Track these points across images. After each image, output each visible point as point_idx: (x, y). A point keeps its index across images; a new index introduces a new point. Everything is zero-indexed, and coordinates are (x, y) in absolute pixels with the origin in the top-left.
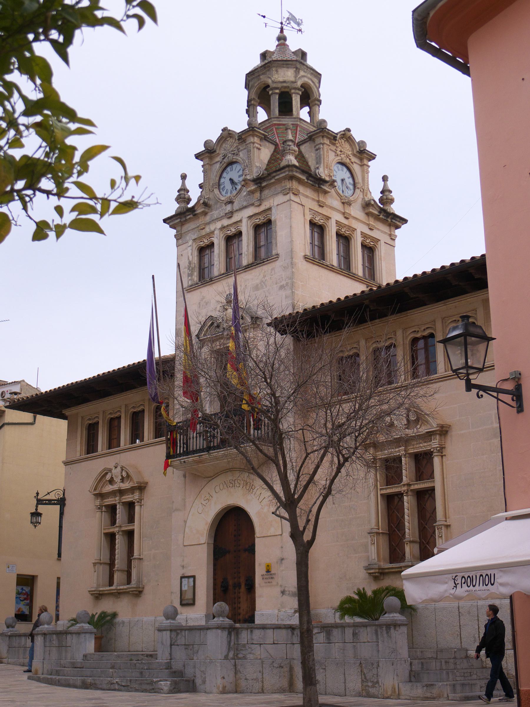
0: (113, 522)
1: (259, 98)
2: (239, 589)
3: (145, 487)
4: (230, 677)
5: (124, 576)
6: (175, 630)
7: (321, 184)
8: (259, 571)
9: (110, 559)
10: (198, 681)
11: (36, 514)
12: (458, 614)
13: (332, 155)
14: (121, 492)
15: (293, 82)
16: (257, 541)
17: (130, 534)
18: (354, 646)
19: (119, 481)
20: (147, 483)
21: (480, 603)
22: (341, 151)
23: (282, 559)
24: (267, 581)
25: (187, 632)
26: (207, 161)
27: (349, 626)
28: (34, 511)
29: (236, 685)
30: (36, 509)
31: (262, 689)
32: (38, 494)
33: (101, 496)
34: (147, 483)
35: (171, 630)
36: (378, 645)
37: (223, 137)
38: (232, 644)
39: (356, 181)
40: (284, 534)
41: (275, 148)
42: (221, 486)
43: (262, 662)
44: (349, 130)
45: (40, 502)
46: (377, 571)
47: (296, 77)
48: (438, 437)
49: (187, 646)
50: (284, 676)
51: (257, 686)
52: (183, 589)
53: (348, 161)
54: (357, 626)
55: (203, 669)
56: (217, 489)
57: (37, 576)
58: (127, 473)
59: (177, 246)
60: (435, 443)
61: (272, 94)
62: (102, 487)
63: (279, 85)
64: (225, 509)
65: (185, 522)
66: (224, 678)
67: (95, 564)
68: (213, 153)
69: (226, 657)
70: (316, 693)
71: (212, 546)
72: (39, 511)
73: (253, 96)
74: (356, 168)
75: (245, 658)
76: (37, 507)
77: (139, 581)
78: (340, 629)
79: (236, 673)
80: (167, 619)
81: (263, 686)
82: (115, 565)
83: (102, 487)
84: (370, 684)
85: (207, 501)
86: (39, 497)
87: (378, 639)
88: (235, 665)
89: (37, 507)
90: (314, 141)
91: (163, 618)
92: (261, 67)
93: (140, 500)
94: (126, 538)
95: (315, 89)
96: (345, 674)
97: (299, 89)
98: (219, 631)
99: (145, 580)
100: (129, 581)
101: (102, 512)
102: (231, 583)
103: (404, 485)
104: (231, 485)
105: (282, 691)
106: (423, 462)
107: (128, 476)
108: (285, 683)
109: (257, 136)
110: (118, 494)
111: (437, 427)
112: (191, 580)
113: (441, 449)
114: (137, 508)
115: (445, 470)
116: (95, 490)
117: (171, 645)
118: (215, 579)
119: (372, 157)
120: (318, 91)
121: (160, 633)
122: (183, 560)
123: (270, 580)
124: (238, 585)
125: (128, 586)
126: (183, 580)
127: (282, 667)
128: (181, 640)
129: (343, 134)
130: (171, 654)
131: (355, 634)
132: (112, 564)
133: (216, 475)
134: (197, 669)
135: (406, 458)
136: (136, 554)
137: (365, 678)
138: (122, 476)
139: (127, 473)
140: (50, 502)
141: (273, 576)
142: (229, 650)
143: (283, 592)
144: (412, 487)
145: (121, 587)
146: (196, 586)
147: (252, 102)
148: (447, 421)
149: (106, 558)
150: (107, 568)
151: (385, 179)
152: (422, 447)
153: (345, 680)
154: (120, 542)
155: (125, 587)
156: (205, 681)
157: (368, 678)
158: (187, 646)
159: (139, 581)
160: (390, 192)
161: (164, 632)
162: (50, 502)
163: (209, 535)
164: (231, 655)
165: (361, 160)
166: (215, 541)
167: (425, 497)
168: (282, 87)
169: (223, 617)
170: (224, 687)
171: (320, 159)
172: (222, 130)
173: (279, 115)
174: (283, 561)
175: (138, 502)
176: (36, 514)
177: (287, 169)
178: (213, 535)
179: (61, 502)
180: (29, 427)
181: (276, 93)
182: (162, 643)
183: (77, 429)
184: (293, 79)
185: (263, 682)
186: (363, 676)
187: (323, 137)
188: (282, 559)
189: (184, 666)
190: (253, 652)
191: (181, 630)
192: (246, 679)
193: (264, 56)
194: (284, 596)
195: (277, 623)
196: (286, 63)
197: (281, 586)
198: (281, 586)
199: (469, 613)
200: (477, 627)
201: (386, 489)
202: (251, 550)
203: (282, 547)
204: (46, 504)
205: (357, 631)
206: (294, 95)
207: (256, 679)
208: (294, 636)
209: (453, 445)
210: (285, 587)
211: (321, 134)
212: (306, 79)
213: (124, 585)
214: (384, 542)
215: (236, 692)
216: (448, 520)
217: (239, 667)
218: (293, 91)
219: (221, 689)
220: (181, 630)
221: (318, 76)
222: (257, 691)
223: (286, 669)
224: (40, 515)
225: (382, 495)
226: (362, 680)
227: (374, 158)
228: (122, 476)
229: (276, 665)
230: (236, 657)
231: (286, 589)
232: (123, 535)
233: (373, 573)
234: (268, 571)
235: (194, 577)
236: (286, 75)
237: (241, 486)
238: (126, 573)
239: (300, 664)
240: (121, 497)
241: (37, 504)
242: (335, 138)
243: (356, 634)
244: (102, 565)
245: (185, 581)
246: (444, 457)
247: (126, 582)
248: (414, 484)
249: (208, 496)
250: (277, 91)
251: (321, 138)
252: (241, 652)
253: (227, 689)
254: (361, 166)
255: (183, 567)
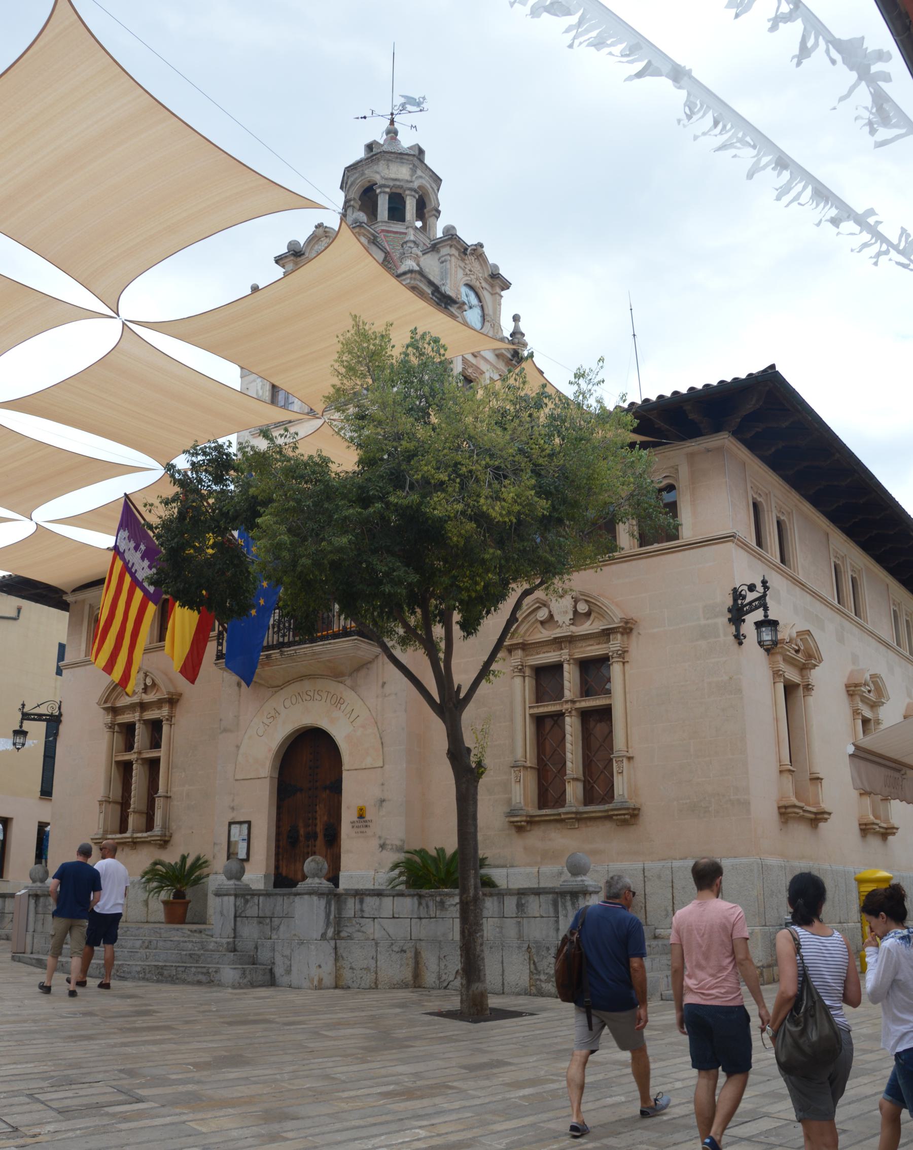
0: (129, 747)
1: (360, 199)
2: (315, 841)
3: (178, 700)
4: (329, 966)
5: (143, 820)
6: (243, 896)
7: (449, 304)
8: (348, 816)
9: (123, 797)
10: (279, 971)
11: (20, 733)
12: (642, 878)
13: (460, 273)
14: (143, 706)
15: (407, 181)
16: (345, 775)
17: (153, 764)
18: (519, 922)
19: (141, 691)
20: (180, 695)
21: (676, 864)
22: (470, 271)
23: (382, 801)
24: (359, 830)
25: (261, 898)
26: (290, 266)
27: (511, 894)
28: (18, 728)
29: (336, 977)
30: (21, 727)
31: (376, 983)
32: (23, 705)
33: (114, 711)
34: (180, 695)
35: (236, 896)
36: (557, 922)
37: (316, 236)
38: (332, 917)
39: (486, 312)
40: (386, 766)
41: (386, 257)
42: (294, 698)
43: (377, 944)
44: (481, 246)
45: (26, 716)
46: (524, 818)
47: (412, 176)
48: (619, 636)
49: (261, 919)
50: (408, 964)
51: (369, 978)
52: (232, 839)
53: (478, 284)
54: (523, 894)
55: (287, 952)
56: (288, 703)
57: (11, 819)
58: (153, 681)
59: (241, 377)
60: (615, 644)
61: (380, 192)
62: (115, 699)
63: (391, 183)
64: (298, 730)
65: (238, 747)
66: (320, 966)
67: (101, 803)
68: (300, 256)
69: (323, 936)
70: (483, 996)
71: (276, 780)
72: (25, 728)
73: (352, 195)
74: (486, 295)
75: (350, 937)
76: (22, 723)
77: (165, 826)
78: (495, 898)
79: (336, 960)
80: (229, 878)
81: (376, 979)
82: (130, 805)
83: (115, 699)
84: (543, 977)
85: (271, 720)
86: (25, 710)
87: (558, 913)
88: (336, 948)
89: (22, 723)
90: (438, 251)
91: (224, 877)
92: (367, 159)
93: (170, 718)
94: (147, 767)
95: (432, 196)
96: (502, 963)
97: (415, 191)
98: (315, 898)
99: (174, 826)
100: (149, 826)
101: (524, 677)
102: (302, 832)
103: (567, 702)
104: (308, 698)
105: (404, 985)
106: (594, 671)
107: (154, 684)
108: (408, 974)
109: (364, 235)
110: (138, 709)
111: (621, 622)
112: (245, 826)
113: (623, 654)
114: (165, 728)
115: (627, 682)
116: (106, 702)
117: (235, 917)
118: (278, 827)
119: (506, 285)
120: (437, 196)
121: (218, 900)
122: (233, 800)
123: (364, 829)
124: (313, 836)
125: (149, 833)
126: (233, 826)
127: (405, 952)
128: (252, 911)
129: (474, 250)
130: (235, 930)
131: (520, 906)
132: (124, 804)
133: (288, 683)
134: (277, 953)
135: (569, 664)
136: (161, 791)
137: (536, 969)
138: (145, 684)
139: (153, 681)
140: (39, 717)
141: (368, 824)
142: (328, 924)
143: (383, 846)
144: (578, 705)
145: (139, 835)
146: (252, 835)
147: (352, 203)
148: (632, 614)
149: (117, 794)
150: (118, 808)
151: (516, 318)
152: (593, 650)
153: (503, 971)
154: (138, 774)
155: (145, 835)
156: (291, 970)
157: (539, 969)
158: (261, 919)
159: (165, 826)
160: (523, 335)
161: (226, 898)
162: (39, 717)
163: (273, 766)
164: (330, 932)
165: (492, 286)
166: (280, 774)
167: (598, 719)
168: (394, 186)
169: (319, 877)
170: (320, 980)
171: (446, 274)
172: (316, 227)
173: (389, 219)
174: (384, 804)
175: (167, 720)
176: (20, 733)
177: (409, 275)
178: (278, 766)
179: (53, 722)
180: (11, 622)
181: (385, 192)
182: (222, 914)
183: (82, 621)
184: (408, 177)
185: (376, 973)
186: (532, 966)
187: (451, 246)
188: (382, 801)
189: (256, 948)
190: (363, 929)
191: (253, 895)
192: (351, 968)
193: (370, 147)
194: (384, 851)
195: (372, 887)
196: (401, 156)
197: (380, 837)
198: (380, 837)
199: (659, 877)
200: (671, 897)
201: (538, 707)
202: (336, 787)
203: (383, 784)
204: (34, 720)
205: (523, 902)
206: (408, 198)
207: (367, 969)
208: (421, 908)
209: (638, 648)
210: (386, 839)
211: (449, 242)
212: (424, 182)
213: (142, 832)
214: (530, 780)
215: (336, 987)
216: (630, 750)
217: (340, 951)
218: (407, 192)
219: (316, 983)
220: (253, 895)
221: (438, 180)
222: (368, 986)
223: (410, 954)
224: (24, 733)
225: (118, 763)
226: (531, 972)
227: (508, 288)
228: (145, 684)
229: (396, 949)
230: (337, 935)
231: (388, 842)
232: (142, 764)
233: (517, 822)
234: (361, 817)
235: (249, 823)
236: (401, 172)
237: (324, 700)
238: (145, 816)
239: (458, 949)
240: (142, 713)
241: (23, 719)
242: (466, 249)
243: (523, 905)
244: (112, 804)
245: (235, 829)
246: (626, 665)
247: (144, 827)
248: (580, 701)
249: (273, 713)
250: (388, 190)
251: (448, 248)
252: (345, 929)
253: (324, 982)
254: (492, 294)
255: (233, 809)
